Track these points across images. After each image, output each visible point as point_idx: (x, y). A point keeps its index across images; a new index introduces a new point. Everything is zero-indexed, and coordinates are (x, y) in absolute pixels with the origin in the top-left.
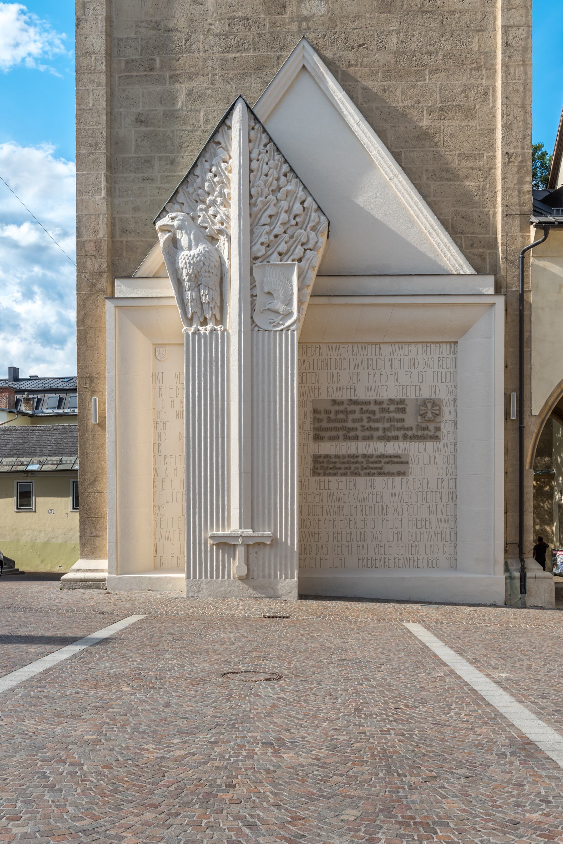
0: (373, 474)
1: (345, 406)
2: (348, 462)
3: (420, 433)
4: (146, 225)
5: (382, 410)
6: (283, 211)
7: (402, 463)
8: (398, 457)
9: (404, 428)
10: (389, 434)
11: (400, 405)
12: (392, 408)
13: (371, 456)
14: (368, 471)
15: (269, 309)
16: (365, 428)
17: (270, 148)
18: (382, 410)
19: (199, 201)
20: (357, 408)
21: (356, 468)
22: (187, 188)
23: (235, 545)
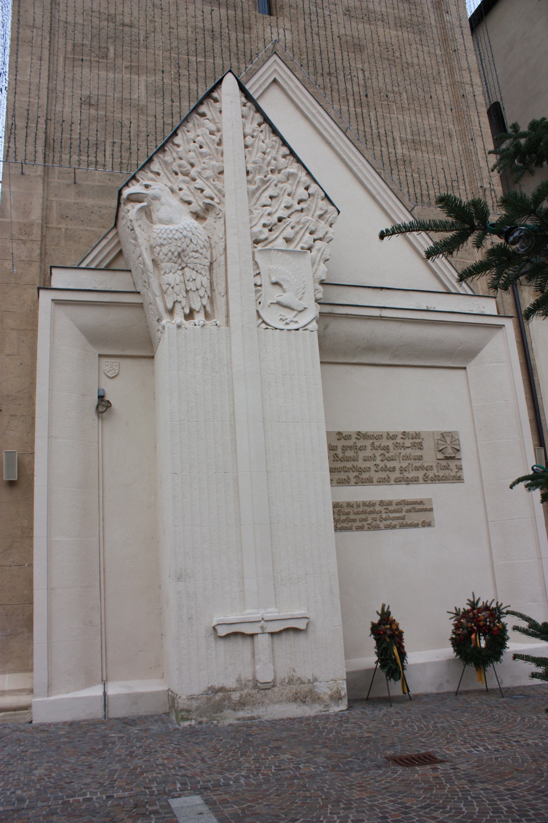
0: (394, 527)
1: (354, 440)
2: (364, 512)
3: (441, 474)
4: (92, 212)
5: (396, 446)
6: (286, 194)
7: (426, 510)
8: (421, 503)
9: (422, 468)
10: (406, 474)
11: (416, 439)
12: (408, 443)
13: (390, 503)
14: (388, 522)
15: (278, 303)
16: (380, 467)
17: (265, 128)
18: (396, 446)
19: (179, 173)
20: (368, 443)
21: (374, 519)
22: (164, 157)
23: (252, 636)
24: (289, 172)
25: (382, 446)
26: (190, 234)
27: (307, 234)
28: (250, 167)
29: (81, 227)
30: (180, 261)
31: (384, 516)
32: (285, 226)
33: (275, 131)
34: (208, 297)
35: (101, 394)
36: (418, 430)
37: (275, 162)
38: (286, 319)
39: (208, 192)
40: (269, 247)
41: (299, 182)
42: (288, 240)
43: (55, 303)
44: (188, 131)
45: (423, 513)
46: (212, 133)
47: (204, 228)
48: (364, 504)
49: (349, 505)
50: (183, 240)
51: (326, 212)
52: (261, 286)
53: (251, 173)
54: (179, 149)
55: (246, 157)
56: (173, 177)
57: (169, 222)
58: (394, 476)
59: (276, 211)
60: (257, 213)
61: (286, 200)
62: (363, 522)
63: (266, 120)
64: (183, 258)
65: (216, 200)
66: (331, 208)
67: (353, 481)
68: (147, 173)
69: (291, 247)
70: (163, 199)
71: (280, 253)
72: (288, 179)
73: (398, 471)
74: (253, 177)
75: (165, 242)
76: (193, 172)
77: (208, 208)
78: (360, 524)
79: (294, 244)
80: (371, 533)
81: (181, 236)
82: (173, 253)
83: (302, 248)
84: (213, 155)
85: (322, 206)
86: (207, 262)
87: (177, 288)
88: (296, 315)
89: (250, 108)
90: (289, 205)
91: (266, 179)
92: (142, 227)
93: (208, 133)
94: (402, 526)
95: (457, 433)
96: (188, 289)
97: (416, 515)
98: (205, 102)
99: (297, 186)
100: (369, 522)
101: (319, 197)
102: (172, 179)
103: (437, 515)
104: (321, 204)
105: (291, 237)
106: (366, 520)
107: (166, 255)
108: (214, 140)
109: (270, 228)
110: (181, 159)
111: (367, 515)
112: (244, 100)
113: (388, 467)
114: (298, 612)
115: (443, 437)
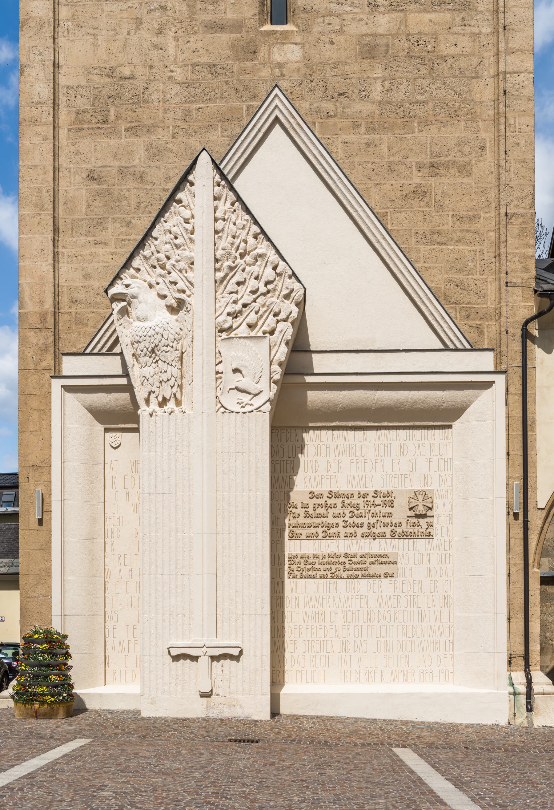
0: (357, 577)
1: (325, 498)
2: (329, 563)
4: (98, 294)
7: (390, 563)
8: (386, 556)
11: (388, 498)
15: (237, 389)
19: (157, 266)
20: (339, 501)
26: (161, 331)
27: (271, 316)
28: (219, 253)
29: (89, 310)
30: (154, 355)
32: (249, 311)
33: (247, 211)
34: (178, 385)
38: (243, 403)
39: (181, 285)
41: (267, 262)
42: (251, 326)
43: (65, 389)
46: (187, 221)
50: (155, 336)
51: (292, 290)
52: (222, 373)
53: (220, 260)
57: (145, 320)
59: (242, 297)
60: (222, 303)
61: (252, 284)
63: (239, 198)
64: (157, 352)
65: (188, 292)
69: (253, 334)
70: (140, 298)
71: (242, 340)
72: (257, 261)
74: (222, 265)
75: (141, 340)
78: (325, 573)
82: (147, 349)
83: (264, 333)
85: (288, 286)
86: (178, 353)
87: (151, 380)
88: (252, 398)
89: (224, 187)
91: (233, 265)
93: (182, 222)
94: (364, 576)
95: (431, 491)
101: (286, 275)
102: (151, 273)
104: (287, 283)
107: (142, 351)
108: (187, 230)
110: (158, 252)
112: (218, 178)
114: (233, 643)
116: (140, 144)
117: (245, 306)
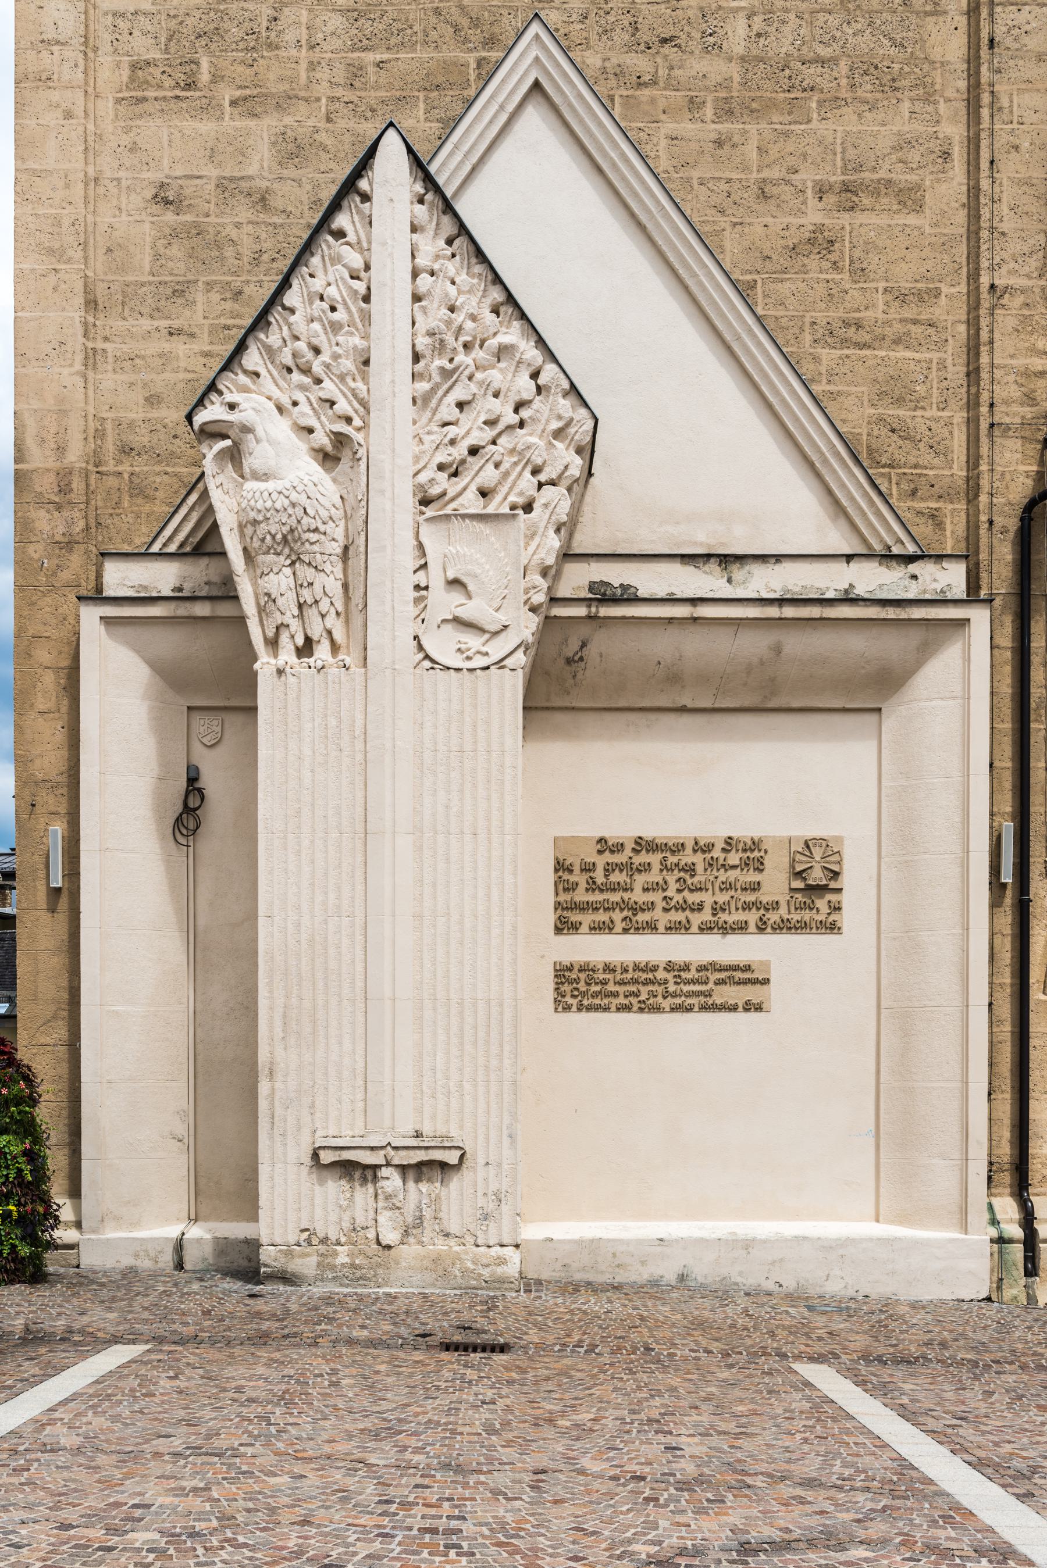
0: (689, 1009)
2: (635, 981)
4: (175, 437)
7: (755, 982)
8: (747, 968)
9: (757, 905)
11: (753, 855)
13: (686, 967)
15: (457, 620)
20: (655, 859)
24: (500, 345)
25: (682, 863)
26: (302, 499)
27: (527, 474)
28: (423, 342)
29: (157, 468)
31: (672, 988)
35: (193, 775)
36: (756, 834)
37: (473, 325)
39: (343, 406)
40: (448, 510)
44: (311, 276)
45: (749, 987)
47: (334, 480)
48: (637, 967)
49: (608, 968)
54: (292, 319)
55: (413, 323)
56: (284, 379)
57: (265, 477)
58: (706, 916)
59: (468, 433)
62: (631, 999)
66: (583, 412)
67: (619, 926)
68: (236, 374)
73: (707, 909)
75: (260, 518)
76: (317, 368)
77: (340, 440)
79: (498, 498)
80: (645, 1017)
81: (286, 502)
82: (273, 537)
84: (355, 325)
90: (493, 417)
92: (225, 487)
94: (704, 1008)
95: (840, 840)
96: (302, 601)
97: (729, 990)
98: (345, 203)
99: (516, 371)
100: (642, 998)
102: (281, 383)
103: (775, 994)
105: (492, 485)
106: (636, 995)
108: (356, 292)
109: (452, 470)
111: (641, 987)
112: (419, 188)
113: (690, 902)
115: (808, 847)
116: (264, 128)
117: (474, 451)
